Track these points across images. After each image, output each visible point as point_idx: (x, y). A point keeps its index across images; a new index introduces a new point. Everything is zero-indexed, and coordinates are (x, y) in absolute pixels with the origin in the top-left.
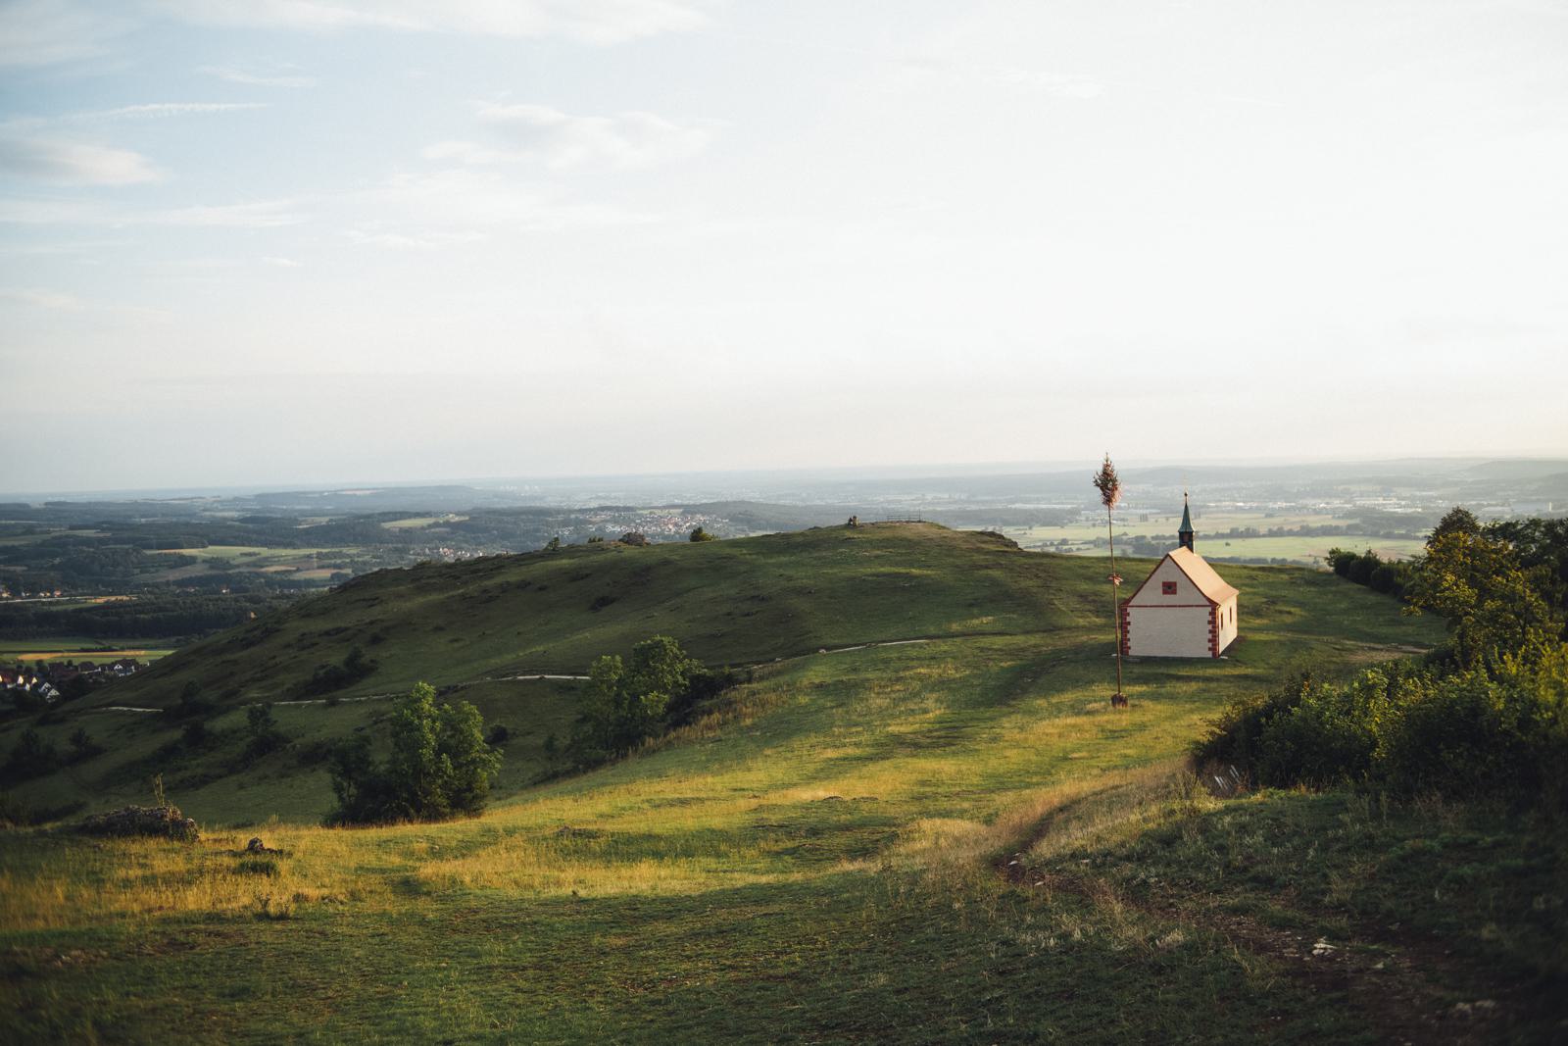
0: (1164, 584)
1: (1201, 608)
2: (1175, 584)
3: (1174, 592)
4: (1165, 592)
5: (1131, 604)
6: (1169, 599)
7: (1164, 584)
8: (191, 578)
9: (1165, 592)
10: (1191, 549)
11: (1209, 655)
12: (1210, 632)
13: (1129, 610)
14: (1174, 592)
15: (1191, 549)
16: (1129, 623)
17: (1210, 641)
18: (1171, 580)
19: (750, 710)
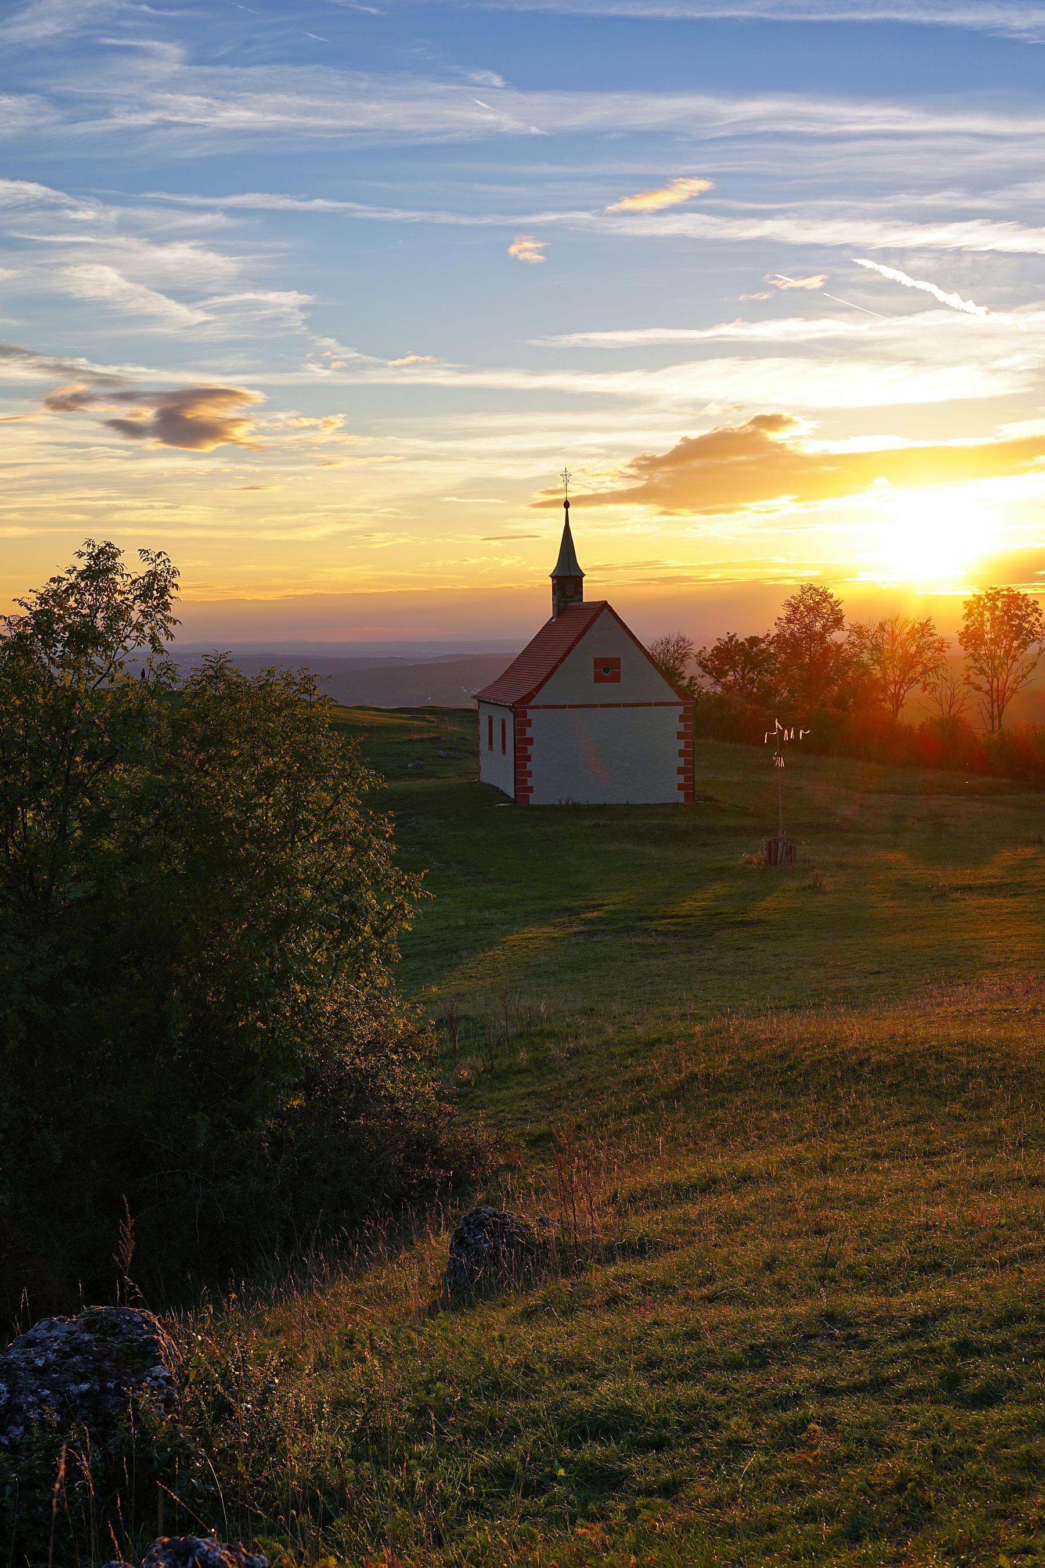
0: (598, 662)
1: (610, 702)
2: (618, 660)
3: (616, 678)
4: (598, 679)
5: (532, 704)
6: (607, 691)
7: (598, 662)
8: (900, 282)
9: (598, 679)
10: (567, 576)
11: (680, 797)
12: (529, 723)
13: (531, 714)
14: (616, 678)
15: (567, 576)
16: (530, 741)
17: (680, 771)
18: (611, 654)
19: (41, 701)
